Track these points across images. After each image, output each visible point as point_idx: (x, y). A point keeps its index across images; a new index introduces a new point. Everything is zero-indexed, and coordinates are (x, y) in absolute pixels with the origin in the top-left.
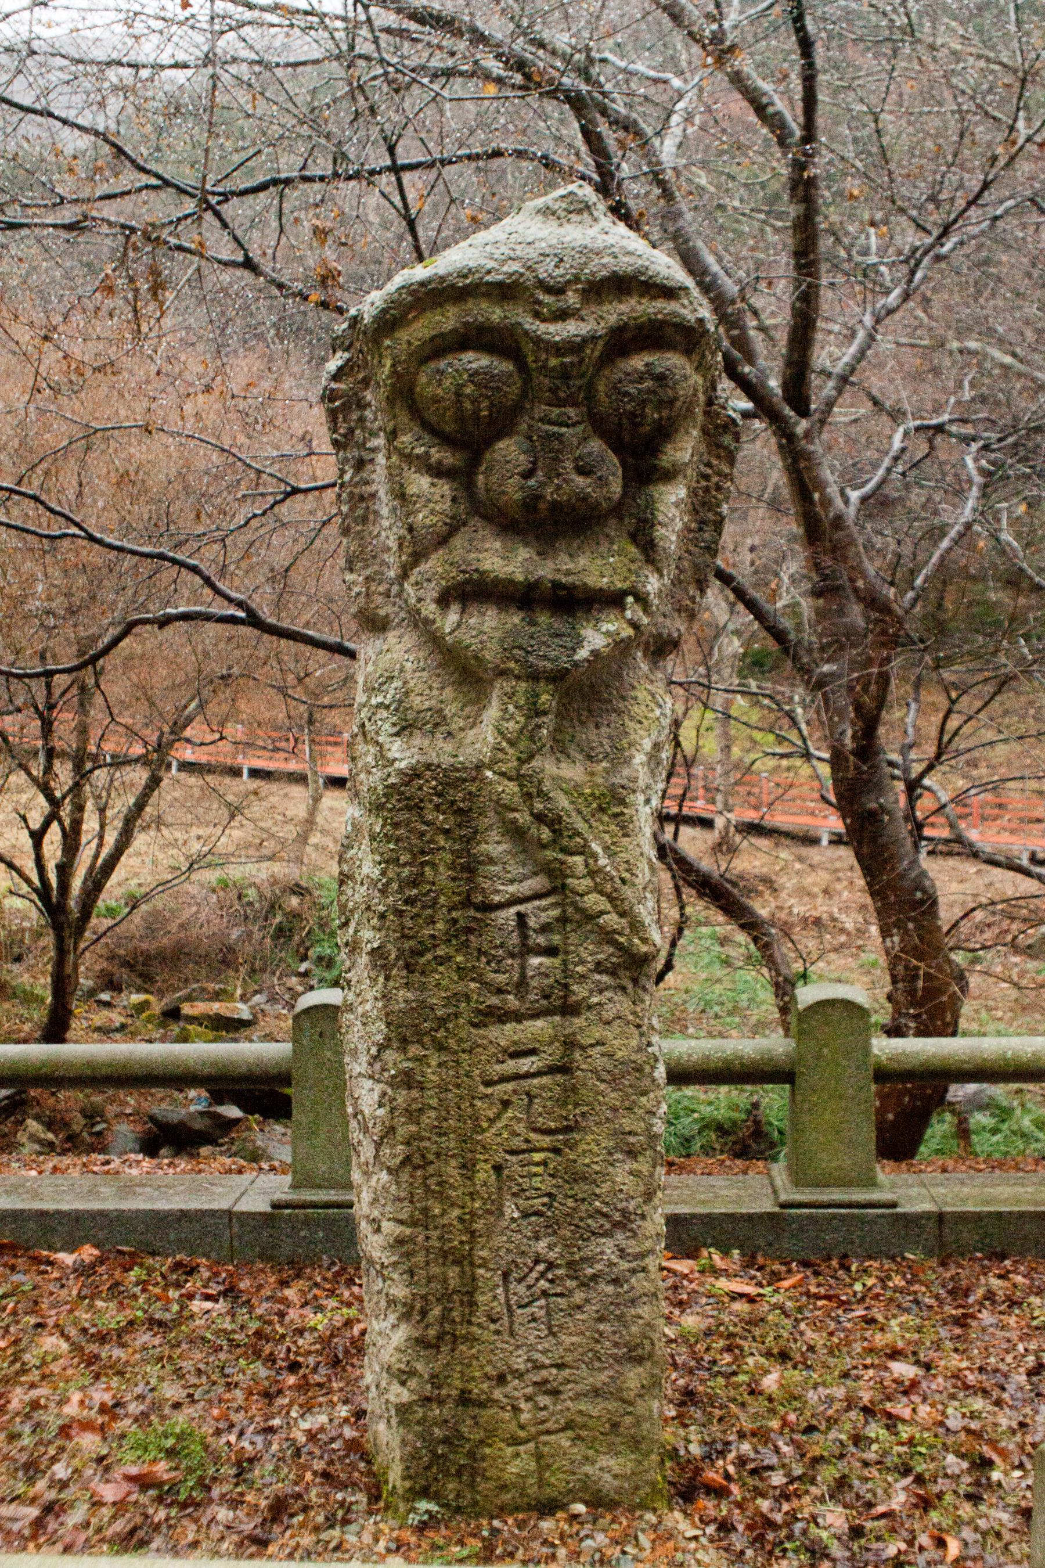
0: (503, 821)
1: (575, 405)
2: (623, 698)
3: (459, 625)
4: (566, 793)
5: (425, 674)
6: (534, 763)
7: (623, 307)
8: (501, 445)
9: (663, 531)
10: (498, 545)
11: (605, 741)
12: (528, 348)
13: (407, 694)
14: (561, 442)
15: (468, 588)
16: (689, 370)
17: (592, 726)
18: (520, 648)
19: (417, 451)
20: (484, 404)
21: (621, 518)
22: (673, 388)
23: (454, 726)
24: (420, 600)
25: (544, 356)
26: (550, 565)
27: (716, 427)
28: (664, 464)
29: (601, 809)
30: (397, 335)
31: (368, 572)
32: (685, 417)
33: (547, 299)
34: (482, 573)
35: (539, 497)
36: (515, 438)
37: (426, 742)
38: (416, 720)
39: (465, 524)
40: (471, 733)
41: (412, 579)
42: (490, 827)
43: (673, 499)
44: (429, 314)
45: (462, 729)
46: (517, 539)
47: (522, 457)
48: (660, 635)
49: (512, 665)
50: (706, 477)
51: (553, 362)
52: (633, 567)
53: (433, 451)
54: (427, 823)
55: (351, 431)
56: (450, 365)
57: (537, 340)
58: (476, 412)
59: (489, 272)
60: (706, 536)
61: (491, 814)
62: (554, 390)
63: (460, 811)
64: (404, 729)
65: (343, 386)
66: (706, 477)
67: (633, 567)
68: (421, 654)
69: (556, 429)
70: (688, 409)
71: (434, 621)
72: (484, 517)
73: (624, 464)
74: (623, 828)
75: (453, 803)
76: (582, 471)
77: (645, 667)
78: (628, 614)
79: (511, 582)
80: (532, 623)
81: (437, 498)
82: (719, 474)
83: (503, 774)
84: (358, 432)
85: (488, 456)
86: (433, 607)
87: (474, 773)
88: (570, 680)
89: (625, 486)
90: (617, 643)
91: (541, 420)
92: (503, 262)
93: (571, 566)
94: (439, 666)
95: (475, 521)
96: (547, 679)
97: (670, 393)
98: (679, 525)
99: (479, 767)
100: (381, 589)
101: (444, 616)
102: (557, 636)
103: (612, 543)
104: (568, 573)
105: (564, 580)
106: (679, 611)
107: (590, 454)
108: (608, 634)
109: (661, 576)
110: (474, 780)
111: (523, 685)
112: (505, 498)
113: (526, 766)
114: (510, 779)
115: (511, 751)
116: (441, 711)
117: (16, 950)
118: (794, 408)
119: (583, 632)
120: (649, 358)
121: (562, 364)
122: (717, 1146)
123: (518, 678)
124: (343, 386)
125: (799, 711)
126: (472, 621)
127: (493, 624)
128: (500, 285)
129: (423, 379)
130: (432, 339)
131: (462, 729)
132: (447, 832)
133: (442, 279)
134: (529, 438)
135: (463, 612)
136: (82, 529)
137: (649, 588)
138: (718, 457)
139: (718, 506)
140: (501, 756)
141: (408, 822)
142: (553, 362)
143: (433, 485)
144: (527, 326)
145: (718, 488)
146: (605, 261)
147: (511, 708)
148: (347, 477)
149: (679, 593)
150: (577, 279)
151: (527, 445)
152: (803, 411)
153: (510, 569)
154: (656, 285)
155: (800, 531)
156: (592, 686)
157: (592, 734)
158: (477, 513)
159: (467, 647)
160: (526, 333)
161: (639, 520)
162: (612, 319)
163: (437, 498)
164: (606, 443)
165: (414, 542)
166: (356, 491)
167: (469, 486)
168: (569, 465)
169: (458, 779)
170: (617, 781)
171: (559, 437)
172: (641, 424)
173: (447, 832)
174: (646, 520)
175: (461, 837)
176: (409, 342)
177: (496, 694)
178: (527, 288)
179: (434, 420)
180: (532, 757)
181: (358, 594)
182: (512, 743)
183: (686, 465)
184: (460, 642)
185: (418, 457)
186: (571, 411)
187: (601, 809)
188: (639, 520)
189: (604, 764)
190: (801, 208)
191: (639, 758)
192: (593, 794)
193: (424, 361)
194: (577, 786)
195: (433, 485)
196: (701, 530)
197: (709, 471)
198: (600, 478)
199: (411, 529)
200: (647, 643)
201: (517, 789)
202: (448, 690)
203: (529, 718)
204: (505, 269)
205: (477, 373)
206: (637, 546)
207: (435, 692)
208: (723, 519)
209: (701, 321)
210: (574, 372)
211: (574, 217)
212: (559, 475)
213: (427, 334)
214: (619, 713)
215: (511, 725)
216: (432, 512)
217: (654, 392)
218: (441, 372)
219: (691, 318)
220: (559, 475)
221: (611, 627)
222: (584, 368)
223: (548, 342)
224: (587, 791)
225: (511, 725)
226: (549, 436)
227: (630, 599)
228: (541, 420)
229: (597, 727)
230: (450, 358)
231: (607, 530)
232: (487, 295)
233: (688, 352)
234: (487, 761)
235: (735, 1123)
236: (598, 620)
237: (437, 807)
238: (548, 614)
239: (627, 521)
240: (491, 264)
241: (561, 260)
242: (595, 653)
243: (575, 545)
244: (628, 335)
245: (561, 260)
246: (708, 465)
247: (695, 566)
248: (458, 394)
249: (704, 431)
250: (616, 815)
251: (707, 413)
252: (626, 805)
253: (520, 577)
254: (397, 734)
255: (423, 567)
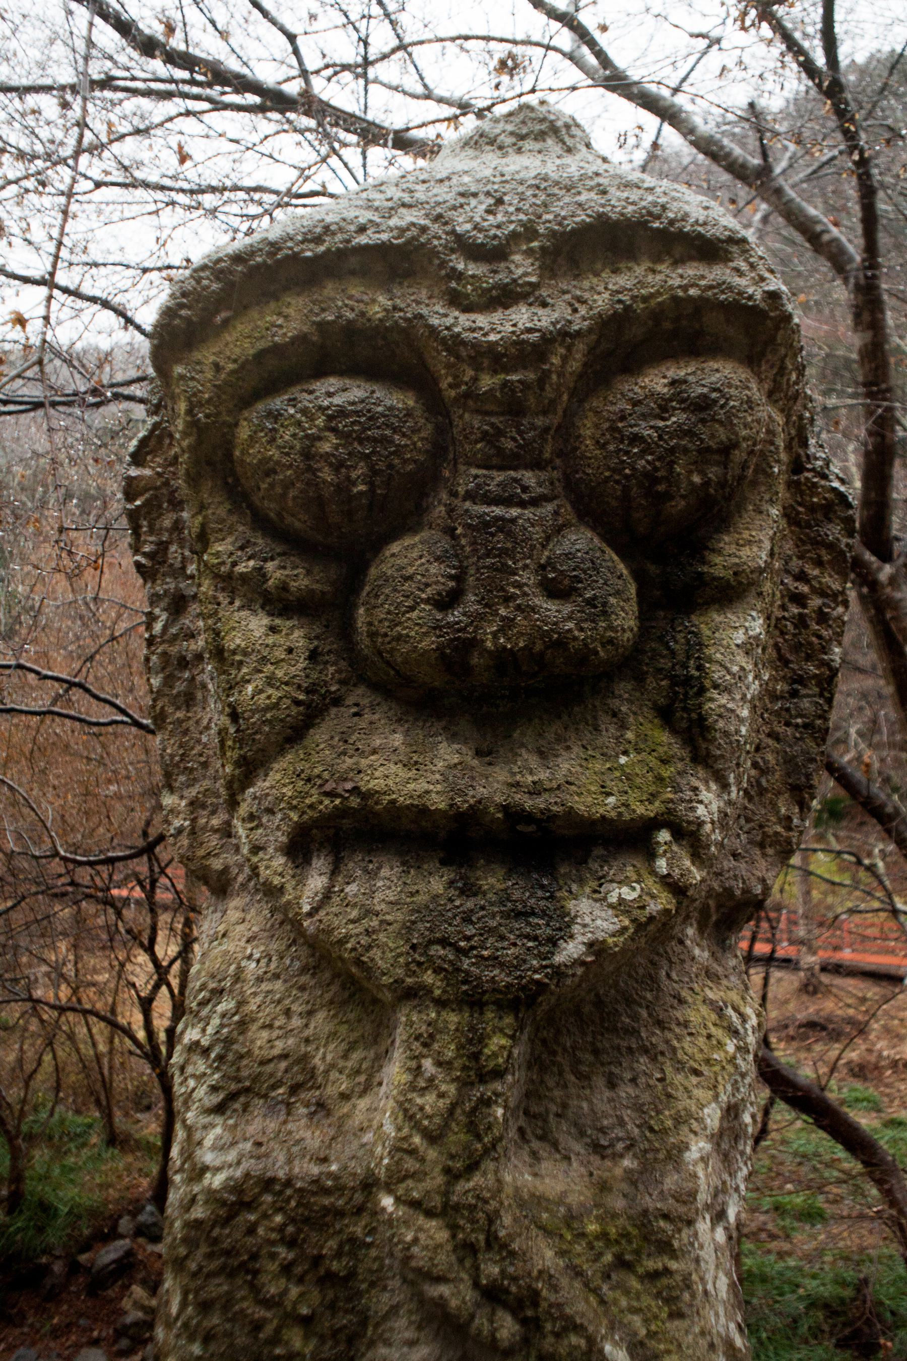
0: (422, 1300)
1: (537, 465)
2: (661, 1024)
3: (327, 895)
4: (547, 1232)
5: (278, 985)
6: (477, 1180)
7: (623, 280)
8: (395, 548)
9: (723, 700)
10: (397, 739)
11: (627, 1114)
12: (438, 361)
13: (243, 1026)
14: (509, 534)
15: (346, 823)
16: (756, 392)
17: (600, 1082)
18: (444, 942)
19: (241, 568)
20: (360, 470)
21: (640, 679)
22: (728, 424)
23: (331, 1091)
24: (256, 849)
25: (470, 373)
26: (501, 775)
27: (812, 509)
28: (719, 572)
29: (622, 1264)
30: (197, 355)
31: (193, 792)
32: (754, 483)
33: (473, 269)
34: (366, 796)
35: (473, 643)
36: (425, 534)
37: (272, 1125)
38: (256, 1078)
39: (337, 701)
40: (363, 1104)
41: (243, 809)
42: (394, 1310)
43: (739, 637)
44: (254, 313)
45: (345, 1097)
46: (439, 726)
47: (434, 569)
48: (729, 891)
49: (429, 978)
50: (799, 599)
51: (487, 382)
52: (667, 772)
53: (270, 566)
54: (268, 1303)
55: (163, 547)
56: (293, 402)
57: (454, 344)
58: (343, 488)
59: (362, 229)
60: (806, 704)
61: (395, 1283)
62: (491, 437)
63: (328, 1279)
64: (232, 1097)
65: (147, 472)
66: (799, 599)
67: (667, 772)
68: (274, 946)
69: (498, 511)
70: (758, 470)
71: (281, 889)
72: (376, 687)
73: (639, 576)
74: (668, 1301)
75: (317, 1260)
76: (553, 591)
77: (701, 954)
78: (662, 865)
79: (423, 811)
80: (469, 890)
81: (280, 654)
82: (822, 593)
83: (415, 1204)
84: (173, 548)
85: (373, 572)
86: (280, 861)
87: (359, 1197)
88: (545, 1003)
89: (644, 616)
90: (640, 927)
91: (470, 496)
92: (391, 212)
93: (543, 775)
94: (304, 970)
95: (359, 695)
96: (500, 1006)
97: (722, 434)
98: (755, 687)
99: (369, 1185)
100: (215, 822)
101: (301, 882)
102: (518, 915)
103: (623, 726)
104: (536, 790)
105: (529, 803)
106: (762, 846)
107: (568, 556)
108: (621, 907)
109: (725, 786)
110: (360, 1210)
111: (453, 1018)
112: (404, 648)
113: (462, 1186)
114: (430, 1214)
115: (432, 1154)
116: (304, 1059)
117: (145, 1102)
118: (874, 553)
119: (571, 905)
120: (674, 371)
121: (505, 384)
122: (826, 1328)
123: (441, 1004)
124: (147, 472)
125: (881, 864)
126: (351, 889)
127: (391, 896)
128: (382, 249)
129: (244, 432)
130: (261, 355)
131: (345, 1097)
132: (306, 1322)
133: (274, 246)
134: (450, 531)
135: (334, 872)
136: (128, 715)
137: (701, 810)
138: (819, 563)
139: (825, 650)
140: (410, 1164)
141: (228, 1302)
142: (487, 382)
143: (273, 629)
144: (435, 321)
145: (822, 617)
146: (582, 198)
147: (428, 1064)
148: (158, 627)
149: (760, 812)
150: (529, 231)
151: (445, 543)
152: (886, 556)
153: (421, 786)
154: (682, 236)
155: (889, 690)
156: (599, 1003)
157: (601, 1098)
158: (362, 679)
159: (342, 942)
160: (433, 331)
161: (675, 681)
162: (602, 302)
163: (280, 654)
164: (603, 537)
165: (240, 741)
166: (174, 650)
167: (346, 630)
168: (527, 577)
169: (326, 1210)
170: (651, 1202)
171: (504, 525)
172: (667, 496)
173: (306, 1322)
174: (688, 681)
175: (335, 1333)
176: (217, 367)
177: (400, 1034)
178: (434, 253)
179: (270, 507)
180: (472, 1167)
181: (180, 831)
182: (432, 1138)
183: (761, 571)
184: (329, 931)
185: (243, 577)
186: (529, 477)
187: (622, 1264)
188: (675, 681)
189: (627, 1163)
190: (869, 335)
191: (698, 1147)
192: (603, 1235)
193: (247, 401)
194: (571, 1219)
195: (273, 629)
196: (794, 694)
197: (805, 589)
198: (591, 602)
199: (234, 716)
200: (704, 913)
201: (443, 1235)
202: (321, 1016)
203: (464, 1084)
204: (393, 222)
205: (342, 413)
206: (674, 731)
207: (296, 1022)
208: (834, 672)
209: (774, 296)
210: (532, 401)
211: (528, 145)
212: (508, 599)
213: (250, 349)
214: (653, 1053)
215: (429, 1101)
216: (270, 681)
217: (689, 433)
218: (275, 416)
219: (757, 292)
220: (508, 599)
221: (629, 895)
222: (549, 393)
223: (476, 345)
224: (592, 1227)
225: (429, 1101)
226: (485, 525)
227: (664, 836)
228: (470, 496)
229: (612, 1085)
230: (295, 391)
231: (615, 703)
232: (363, 274)
233: (752, 360)
234: (382, 1173)
235: (842, 1301)
236: (601, 880)
237: (286, 1269)
238: (501, 873)
239: (651, 683)
240: (365, 216)
241: (500, 201)
242: (596, 947)
243: (550, 736)
244: (636, 332)
245: (500, 201)
246: (802, 577)
247: (789, 760)
248: (307, 455)
249: (789, 515)
250: (654, 1276)
251: (793, 486)
252: (674, 1254)
253: (438, 802)
254: (219, 1109)
255: (261, 786)
